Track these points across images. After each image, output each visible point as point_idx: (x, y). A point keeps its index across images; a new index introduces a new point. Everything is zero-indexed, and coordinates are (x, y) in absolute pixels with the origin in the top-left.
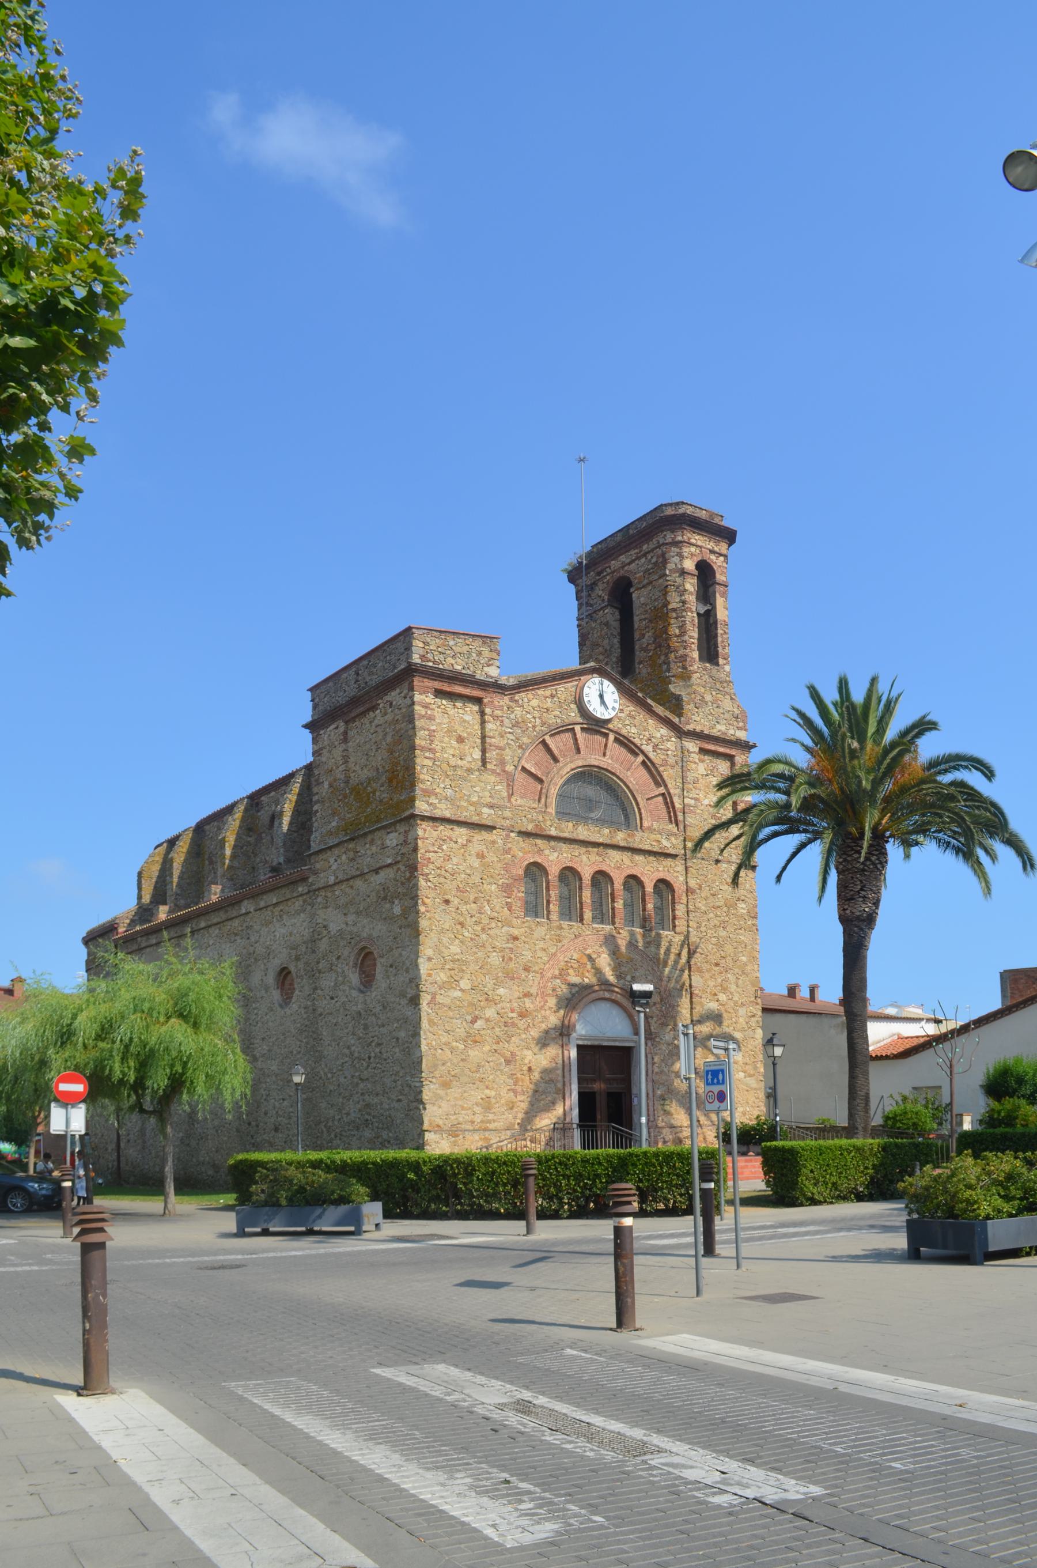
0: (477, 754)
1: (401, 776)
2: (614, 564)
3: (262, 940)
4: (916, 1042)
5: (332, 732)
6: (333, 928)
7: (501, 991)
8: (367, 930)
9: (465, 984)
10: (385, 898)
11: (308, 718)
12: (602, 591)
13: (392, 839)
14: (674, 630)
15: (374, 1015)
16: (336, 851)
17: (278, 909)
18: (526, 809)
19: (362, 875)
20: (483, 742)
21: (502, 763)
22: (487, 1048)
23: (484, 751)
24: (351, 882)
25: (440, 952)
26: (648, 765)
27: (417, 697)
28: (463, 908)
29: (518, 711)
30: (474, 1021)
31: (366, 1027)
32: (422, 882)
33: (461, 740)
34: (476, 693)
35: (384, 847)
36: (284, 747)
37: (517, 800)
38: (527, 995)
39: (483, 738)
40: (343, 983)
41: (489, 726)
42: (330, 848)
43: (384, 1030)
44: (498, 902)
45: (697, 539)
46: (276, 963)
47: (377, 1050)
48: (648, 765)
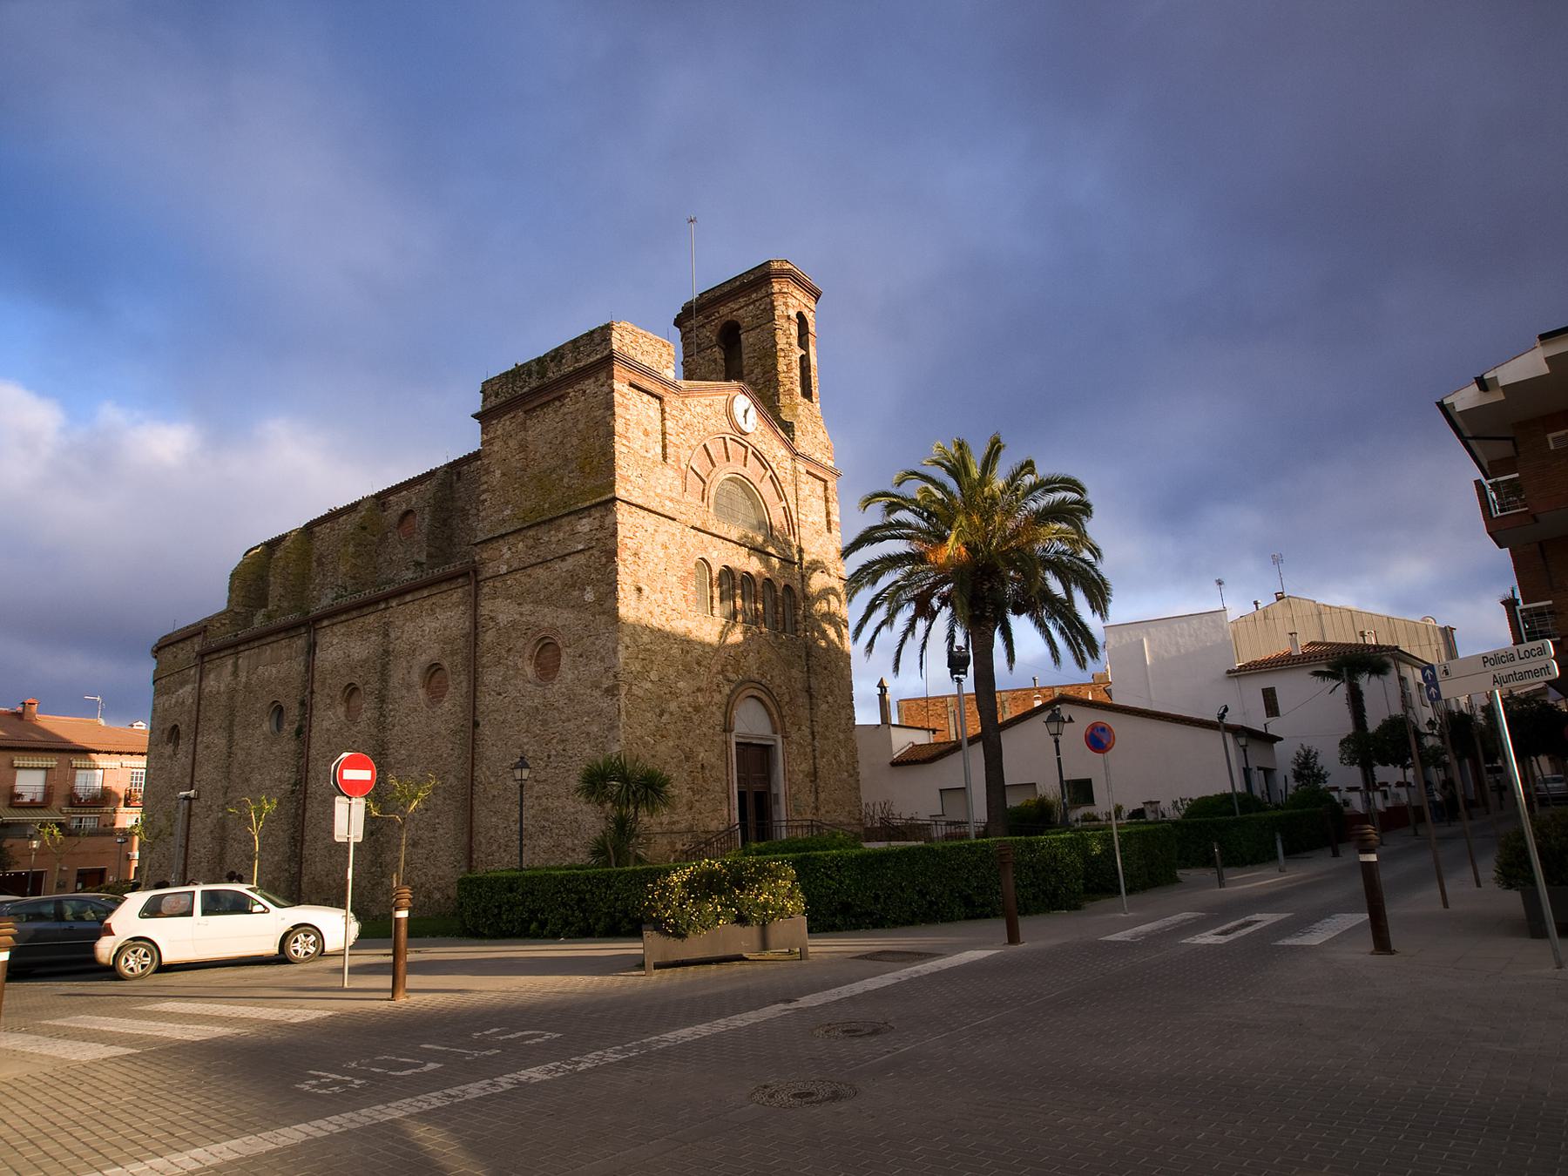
0: (659, 450)
1: (601, 463)
2: (723, 310)
3: (405, 636)
4: (943, 748)
5: (503, 425)
6: (503, 619)
7: (681, 684)
8: (548, 619)
9: (653, 676)
10: (573, 586)
11: (478, 409)
12: (710, 333)
13: (584, 525)
14: (781, 367)
15: (557, 709)
16: (511, 539)
17: (430, 601)
18: (692, 509)
19: (545, 561)
20: (664, 439)
21: (678, 460)
22: (671, 744)
23: (664, 447)
24: (529, 571)
25: (635, 641)
26: (774, 479)
27: (617, 386)
28: (653, 597)
29: (687, 415)
30: (661, 715)
31: (545, 723)
32: (621, 568)
33: (646, 433)
34: (659, 391)
35: (574, 533)
36: (443, 434)
37: (688, 498)
38: (699, 690)
39: (664, 434)
40: (515, 677)
41: (668, 423)
42: (502, 536)
43: (571, 725)
44: (678, 593)
45: (798, 294)
46: (424, 659)
47: (560, 748)
48: (774, 479)
